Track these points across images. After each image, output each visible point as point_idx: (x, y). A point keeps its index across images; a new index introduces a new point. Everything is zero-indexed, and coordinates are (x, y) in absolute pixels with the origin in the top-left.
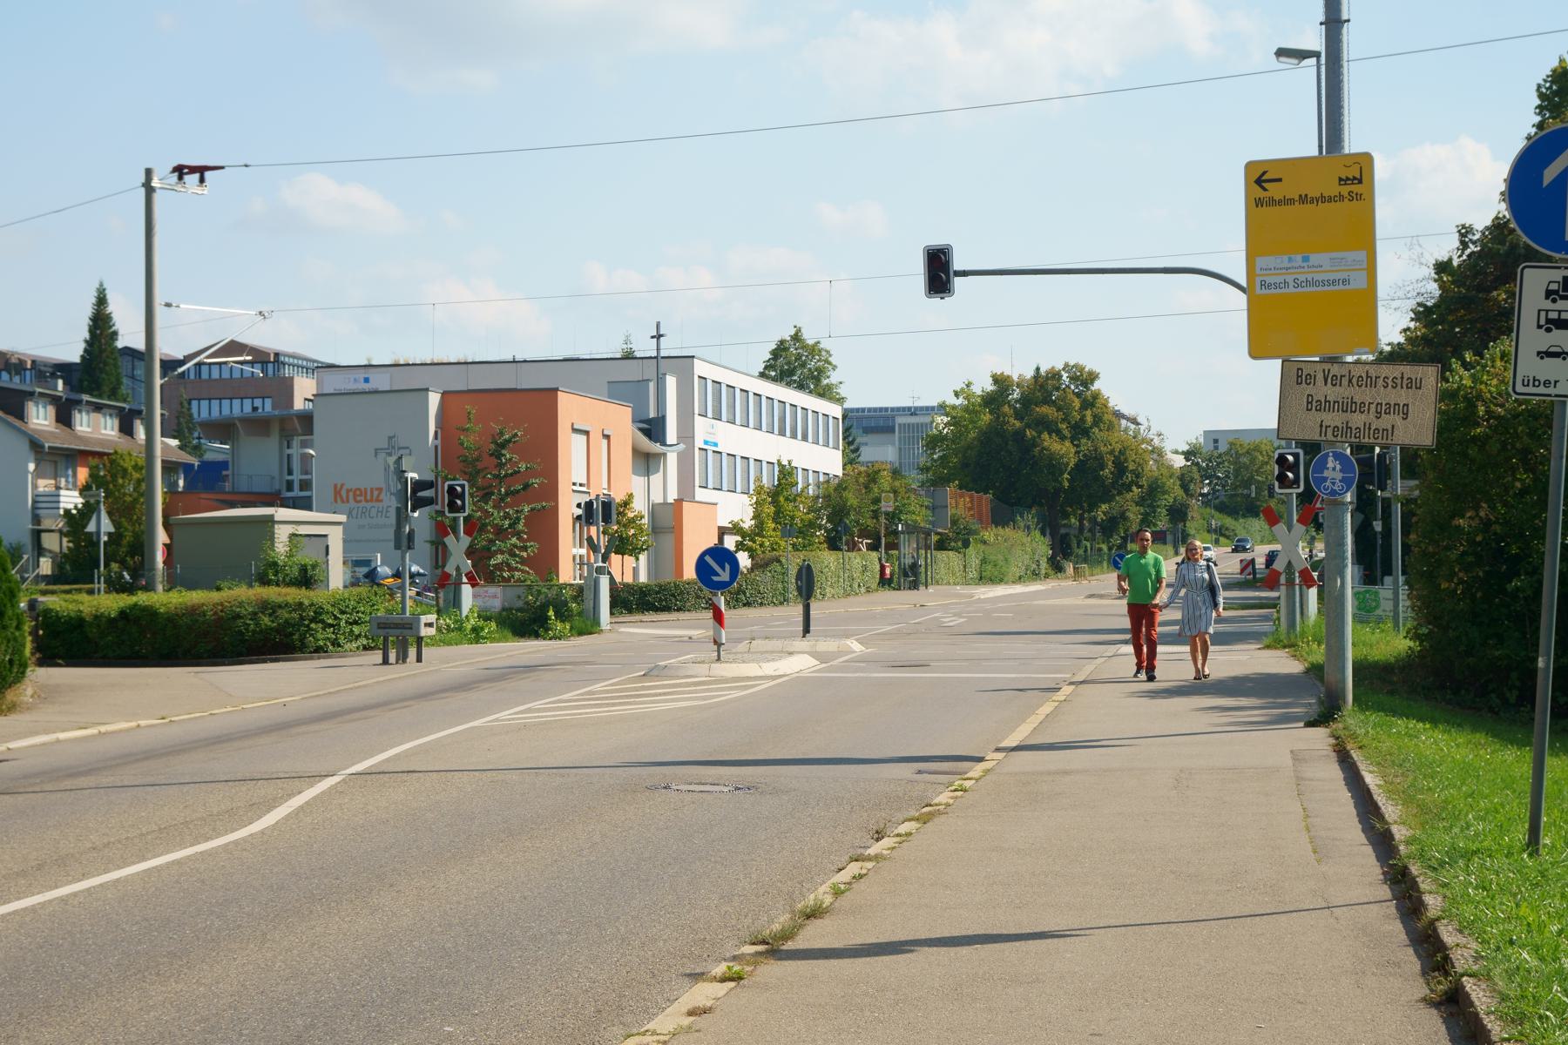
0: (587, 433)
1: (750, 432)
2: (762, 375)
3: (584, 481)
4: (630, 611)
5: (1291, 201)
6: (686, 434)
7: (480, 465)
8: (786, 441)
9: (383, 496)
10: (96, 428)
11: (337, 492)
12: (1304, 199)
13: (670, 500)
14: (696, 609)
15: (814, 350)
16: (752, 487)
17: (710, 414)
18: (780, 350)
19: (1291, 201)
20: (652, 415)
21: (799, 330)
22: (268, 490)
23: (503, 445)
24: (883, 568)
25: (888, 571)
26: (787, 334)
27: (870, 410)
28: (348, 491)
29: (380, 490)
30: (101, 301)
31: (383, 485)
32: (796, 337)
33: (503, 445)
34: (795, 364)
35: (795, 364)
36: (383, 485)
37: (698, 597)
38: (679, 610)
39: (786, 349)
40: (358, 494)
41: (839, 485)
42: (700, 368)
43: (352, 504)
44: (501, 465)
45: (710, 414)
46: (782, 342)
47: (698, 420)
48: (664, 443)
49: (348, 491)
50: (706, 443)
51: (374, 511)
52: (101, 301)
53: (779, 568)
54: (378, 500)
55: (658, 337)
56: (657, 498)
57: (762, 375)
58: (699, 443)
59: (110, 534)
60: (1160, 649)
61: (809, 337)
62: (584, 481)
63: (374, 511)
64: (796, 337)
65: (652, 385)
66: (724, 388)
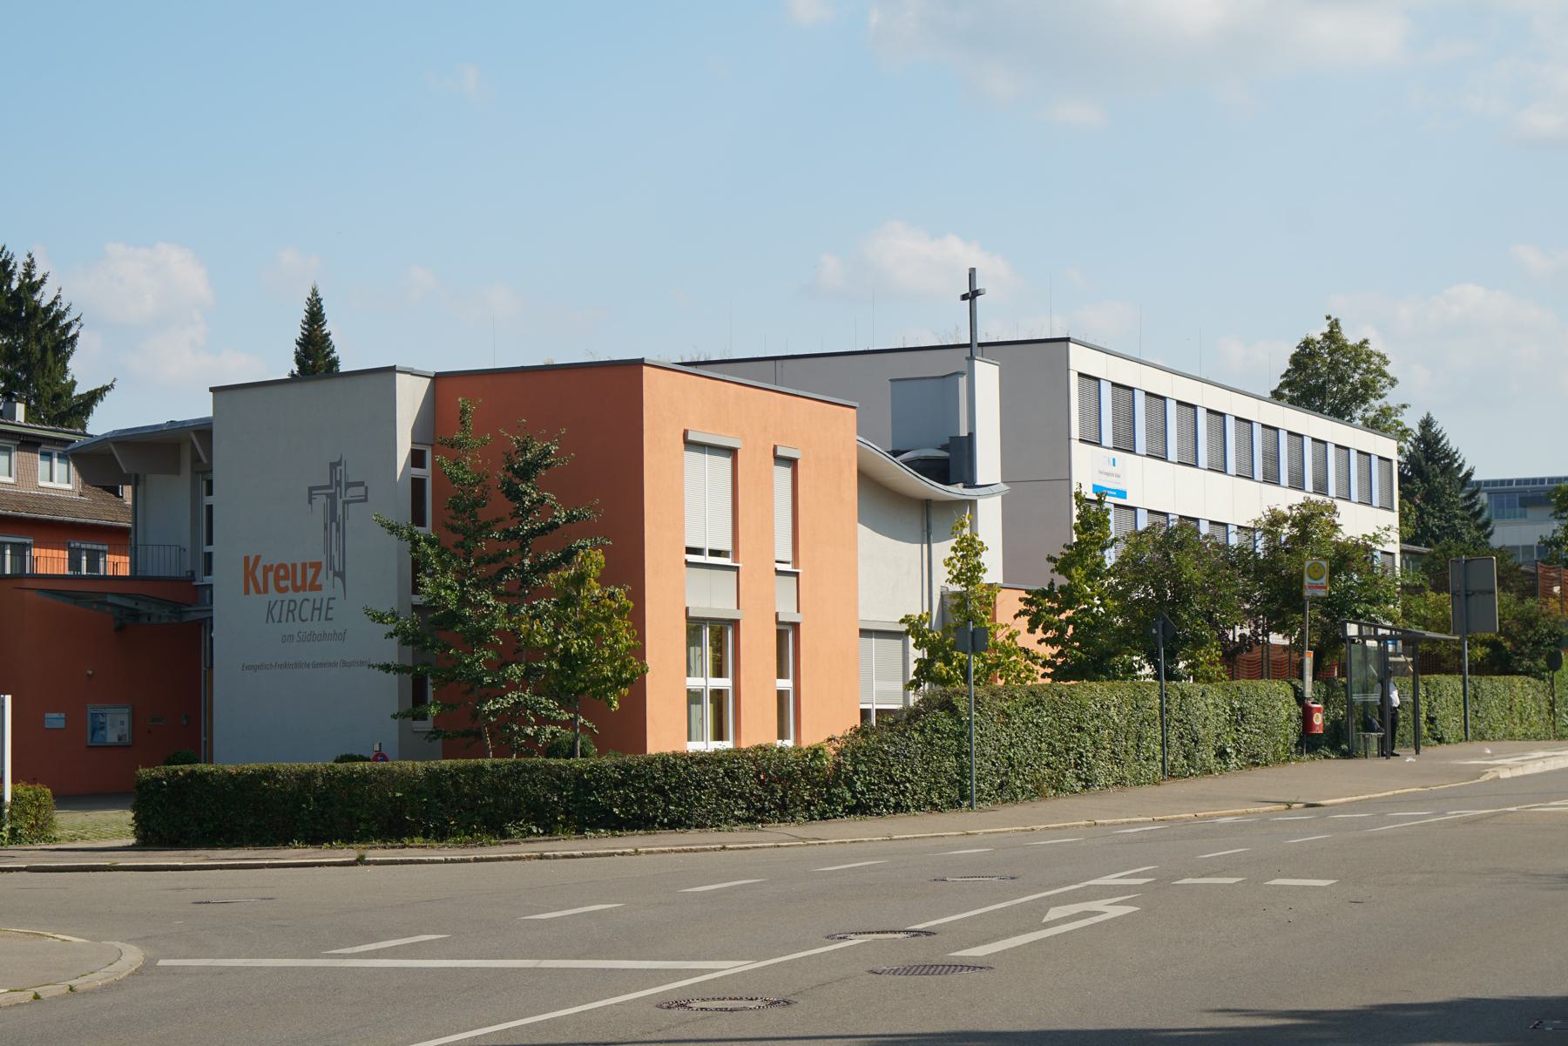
0: (732, 452)
2: (1277, 396)
3: (728, 546)
4: (549, 830)
5: (335, 664)
7: (484, 515)
9: (321, 580)
10: (30, 474)
11: (249, 574)
12: (345, 664)
14: (717, 824)
15: (1360, 353)
17: (1107, 439)
18: (1304, 358)
19: (335, 664)
20: (964, 433)
21: (1335, 325)
22: (173, 572)
23: (525, 473)
24: (1307, 716)
25: (1318, 719)
26: (1317, 332)
27: (1519, 482)
28: (267, 569)
30: (315, 316)
31: (323, 559)
32: (1332, 336)
33: (525, 473)
34: (1327, 377)
35: (1327, 377)
36: (323, 559)
37: (727, 794)
38: (674, 824)
39: (1312, 355)
40: (283, 573)
41: (1169, 534)
42: (1081, 360)
43: (273, 594)
44: (522, 514)
45: (1107, 439)
46: (1307, 343)
48: (970, 483)
49: (267, 569)
52: (315, 316)
53: (946, 723)
55: (972, 295)
57: (1277, 396)
58: (1075, 488)
59: (919, 661)
61: (1351, 337)
62: (727, 546)
63: (307, 607)
64: (1332, 336)
65: (963, 381)
66: (1331, 450)
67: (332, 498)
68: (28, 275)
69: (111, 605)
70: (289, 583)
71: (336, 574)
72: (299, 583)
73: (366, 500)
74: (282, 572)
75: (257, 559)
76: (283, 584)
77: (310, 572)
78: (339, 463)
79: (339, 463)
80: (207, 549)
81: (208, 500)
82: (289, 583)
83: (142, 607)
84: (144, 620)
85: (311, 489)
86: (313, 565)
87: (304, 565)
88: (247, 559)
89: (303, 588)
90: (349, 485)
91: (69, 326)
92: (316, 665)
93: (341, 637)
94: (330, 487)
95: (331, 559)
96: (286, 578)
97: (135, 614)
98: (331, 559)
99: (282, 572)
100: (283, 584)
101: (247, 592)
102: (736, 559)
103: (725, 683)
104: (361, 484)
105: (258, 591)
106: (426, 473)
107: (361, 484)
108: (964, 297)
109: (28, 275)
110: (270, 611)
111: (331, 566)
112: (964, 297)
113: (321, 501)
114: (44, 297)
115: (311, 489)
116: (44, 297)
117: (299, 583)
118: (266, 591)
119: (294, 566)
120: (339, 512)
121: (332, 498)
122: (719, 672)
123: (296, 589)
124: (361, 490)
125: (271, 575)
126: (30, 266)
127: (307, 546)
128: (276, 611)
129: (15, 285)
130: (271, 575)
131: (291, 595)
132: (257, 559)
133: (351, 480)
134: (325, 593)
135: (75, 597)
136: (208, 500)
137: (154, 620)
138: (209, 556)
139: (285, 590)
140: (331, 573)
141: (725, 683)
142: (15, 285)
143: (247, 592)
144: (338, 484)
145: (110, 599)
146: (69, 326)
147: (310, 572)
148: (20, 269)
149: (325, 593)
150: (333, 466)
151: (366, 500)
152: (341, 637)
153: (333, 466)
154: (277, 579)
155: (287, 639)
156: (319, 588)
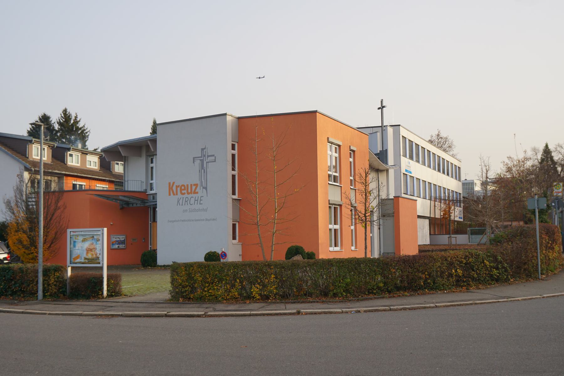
1: (426, 168)
5: (203, 220)
6: (397, 164)
8: (440, 175)
11: (170, 188)
12: (207, 220)
13: (391, 197)
16: (433, 197)
19: (203, 220)
28: (177, 187)
29: (196, 185)
31: (199, 183)
40: (183, 188)
47: (403, 158)
49: (177, 187)
50: (406, 171)
51: (192, 201)
54: (195, 193)
56: (384, 196)
58: (403, 171)
60: (126, 189)
61: (443, 135)
63: (192, 201)
67: (202, 161)
68: (76, 119)
69: (121, 200)
70: (185, 191)
71: (203, 188)
72: (189, 191)
73: (215, 161)
74: (183, 188)
75: (174, 183)
76: (183, 192)
77: (194, 188)
78: (205, 149)
79: (205, 149)
80: (151, 182)
81: (151, 165)
82: (185, 191)
83: (131, 200)
84: (131, 206)
85: (194, 158)
86: (194, 185)
87: (191, 185)
88: (170, 183)
89: (191, 193)
90: (208, 156)
91: (87, 133)
92: (196, 220)
93: (206, 210)
94: (201, 157)
95: (202, 182)
96: (184, 189)
97: (128, 203)
98: (202, 182)
99: (183, 188)
100: (183, 192)
101: (170, 195)
102: (340, 183)
103: (337, 227)
104: (213, 156)
105: (174, 195)
106: (235, 152)
107: (213, 156)
108: (379, 109)
109: (76, 119)
110: (178, 201)
111: (202, 185)
112: (379, 109)
113: (198, 162)
114: (80, 125)
115: (194, 158)
116: (80, 125)
117: (189, 191)
118: (177, 194)
119: (188, 185)
120: (205, 166)
121: (202, 161)
122: (335, 223)
123: (188, 193)
124: (213, 158)
125: (179, 189)
126: (76, 117)
127: (193, 178)
128: (181, 202)
129: (72, 122)
130: (179, 189)
131: (186, 195)
132: (174, 183)
133: (209, 154)
134: (199, 195)
135: (107, 197)
136: (151, 165)
137: (135, 205)
138: (151, 184)
139: (184, 194)
140: (202, 188)
141: (337, 227)
142: (72, 122)
143: (170, 195)
144: (205, 156)
145: (121, 198)
146: (87, 133)
147: (194, 188)
148: (73, 118)
149: (199, 195)
150: (202, 149)
151: (215, 161)
152: (206, 210)
153: (202, 149)
154: (181, 190)
155: (185, 211)
156: (197, 193)
